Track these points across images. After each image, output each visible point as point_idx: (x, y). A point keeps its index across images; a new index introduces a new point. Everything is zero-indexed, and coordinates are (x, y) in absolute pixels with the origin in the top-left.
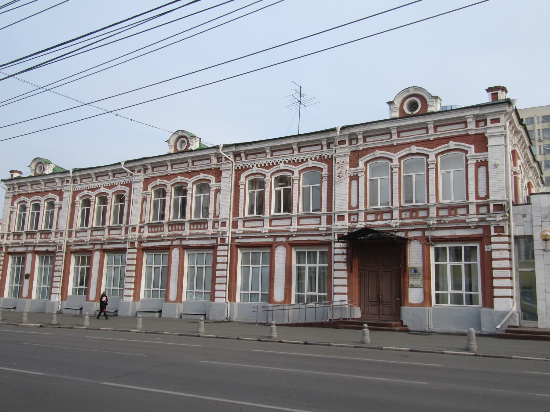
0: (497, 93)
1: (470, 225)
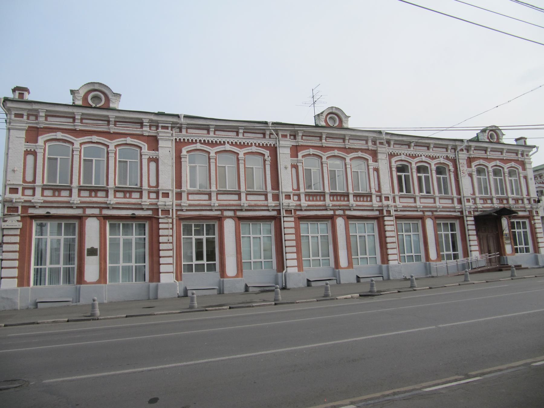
0: (23, 94)
1: (35, 205)
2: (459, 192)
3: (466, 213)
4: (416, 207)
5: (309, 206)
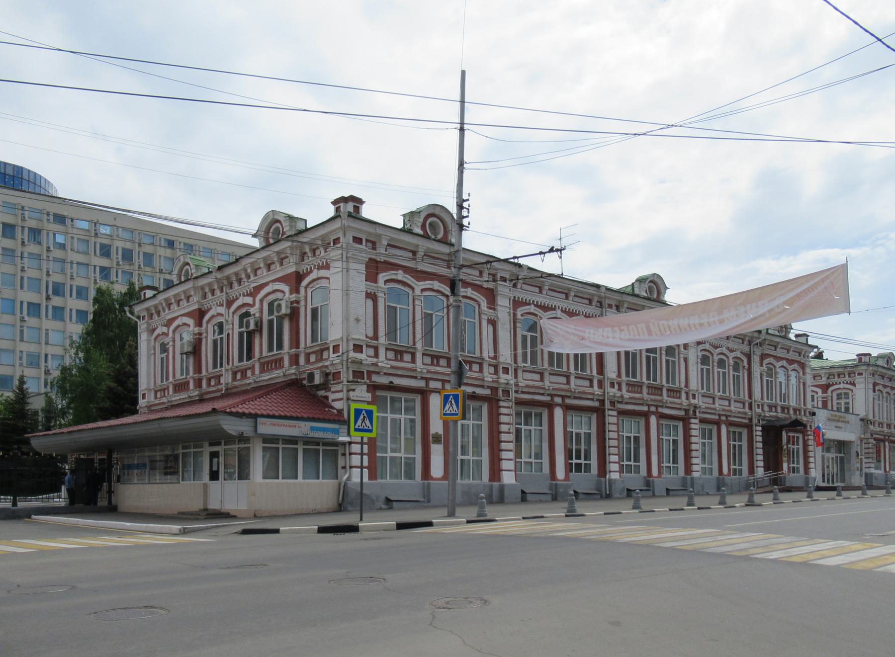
2: (750, 397)
3: (755, 421)
4: (415, 370)
5: (630, 398)
